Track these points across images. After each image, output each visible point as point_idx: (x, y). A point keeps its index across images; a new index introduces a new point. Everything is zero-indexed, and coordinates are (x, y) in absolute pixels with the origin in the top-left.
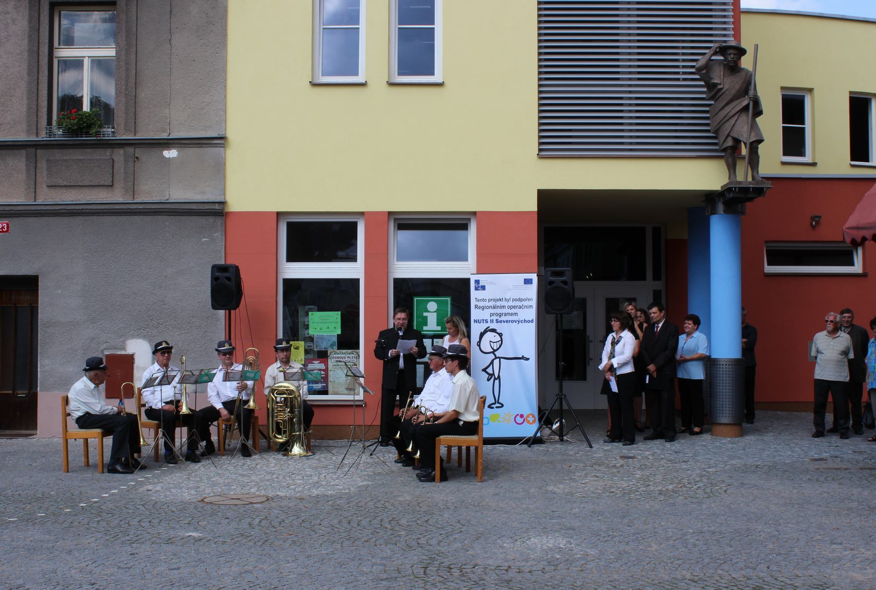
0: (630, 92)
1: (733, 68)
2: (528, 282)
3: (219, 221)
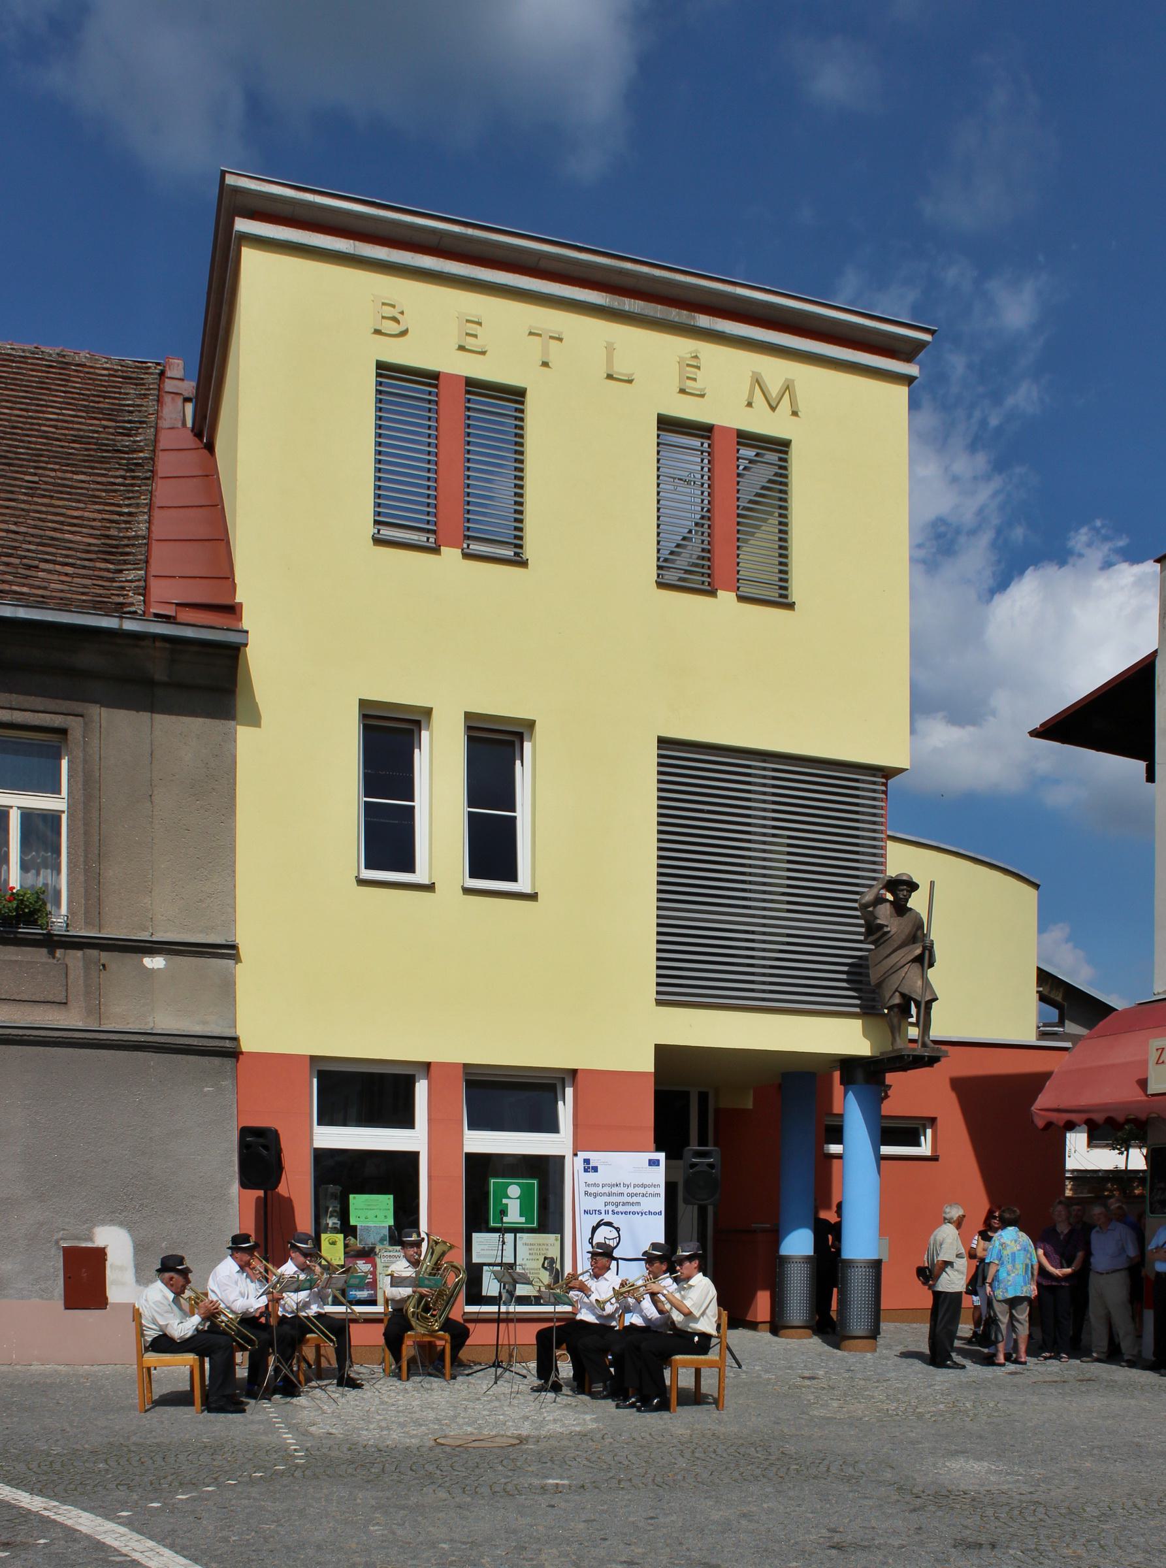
1: (900, 908)
2: (654, 1163)
3: (229, 1063)
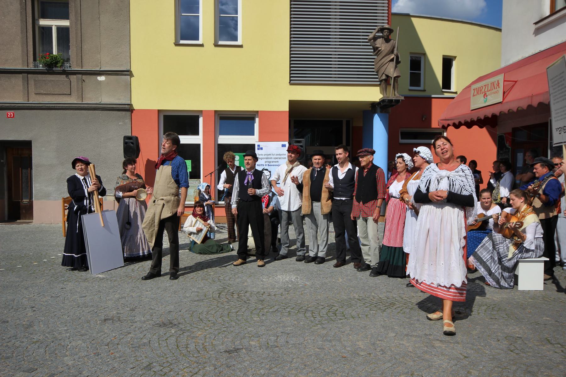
0: (335, 51)
2: (284, 146)
3: (128, 113)
